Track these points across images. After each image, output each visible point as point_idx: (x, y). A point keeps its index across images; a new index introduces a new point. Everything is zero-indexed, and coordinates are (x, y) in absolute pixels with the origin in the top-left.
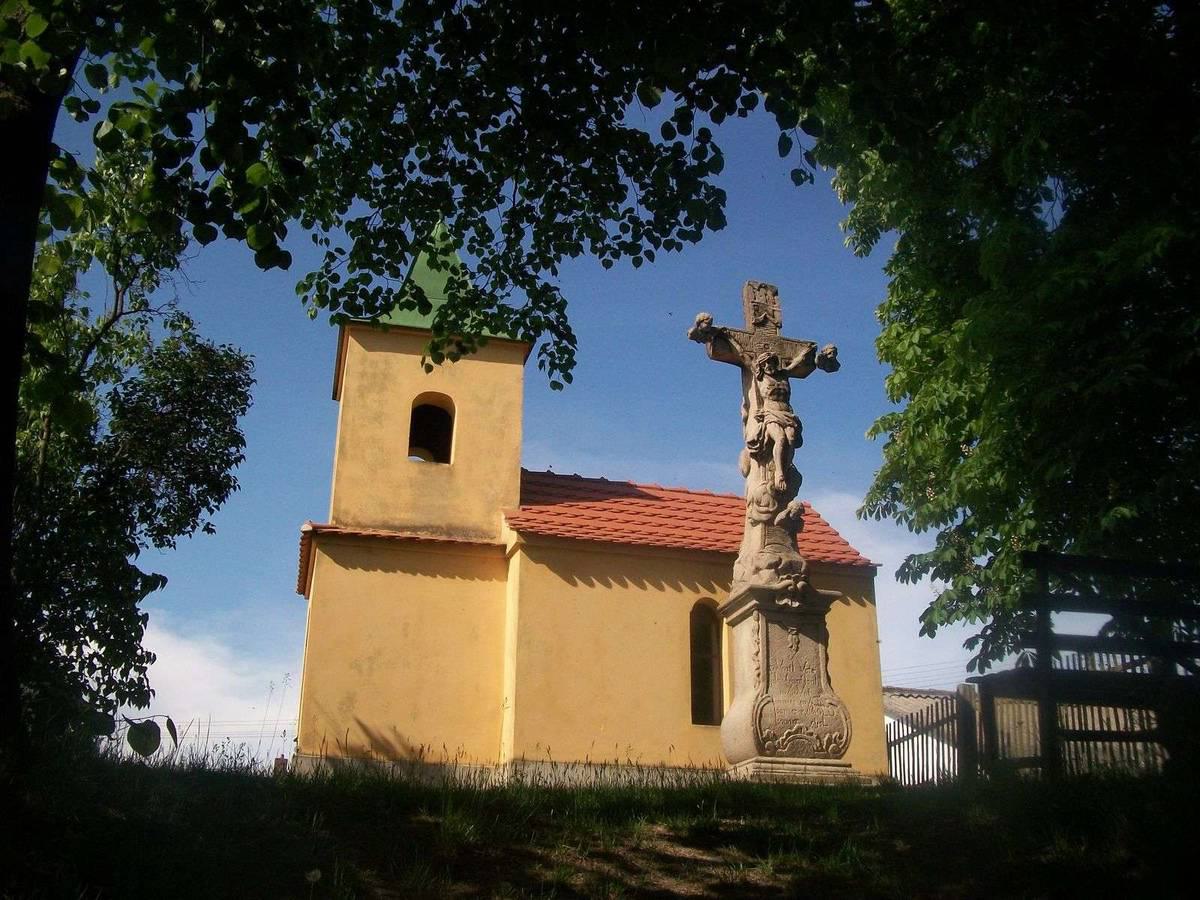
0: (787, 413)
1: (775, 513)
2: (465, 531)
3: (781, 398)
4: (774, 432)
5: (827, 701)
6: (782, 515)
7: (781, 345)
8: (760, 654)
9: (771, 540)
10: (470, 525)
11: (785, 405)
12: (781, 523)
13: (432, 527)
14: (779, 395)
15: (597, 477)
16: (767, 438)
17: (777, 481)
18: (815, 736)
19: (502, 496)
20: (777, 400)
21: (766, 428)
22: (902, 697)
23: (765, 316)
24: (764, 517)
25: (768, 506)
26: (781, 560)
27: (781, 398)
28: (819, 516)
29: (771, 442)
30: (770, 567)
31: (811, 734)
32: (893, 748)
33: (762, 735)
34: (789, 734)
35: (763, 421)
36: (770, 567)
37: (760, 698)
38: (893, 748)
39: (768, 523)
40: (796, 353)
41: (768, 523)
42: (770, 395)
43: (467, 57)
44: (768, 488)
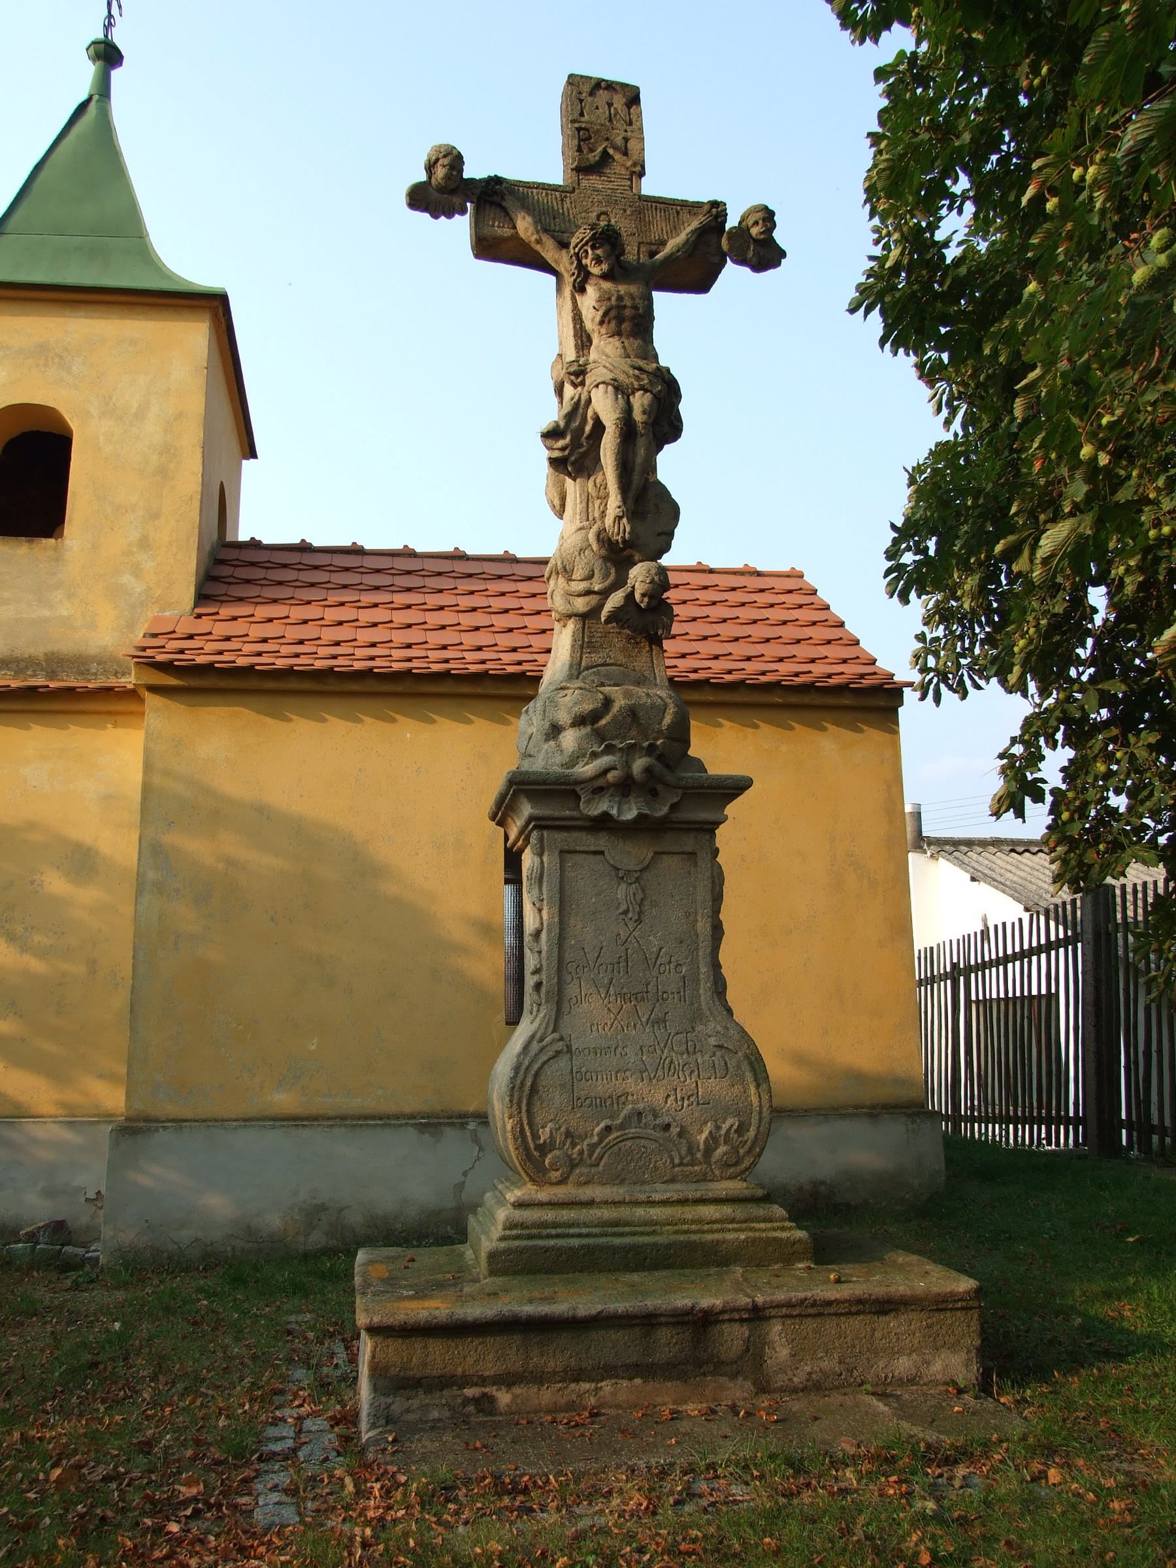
0: (641, 363)
1: (605, 593)
2: (80, 663)
3: (626, 326)
4: (604, 406)
5: (712, 1041)
6: (615, 600)
7: (639, 212)
8: (544, 936)
9: (596, 658)
10: (93, 651)
11: (637, 343)
12: (614, 617)
13: (17, 661)
14: (620, 320)
15: (735, 562)
16: (590, 423)
17: (609, 521)
18: (675, 1130)
19: (159, 592)
20: (618, 333)
21: (589, 401)
22: (1013, 854)
23: (605, 151)
24: (581, 605)
25: (590, 577)
26: (608, 702)
27: (626, 326)
28: (815, 592)
29: (599, 428)
30: (579, 721)
31: (667, 1127)
32: (973, 975)
33: (536, 1136)
34: (608, 1129)
35: (583, 384)
36: (579, 721)
37: (535, 1047)
38: (973, 975)
39: (587, 617)
40: (675, 230)
41: (587, 617)
42: (601, 323)
43: (963, 384)
44: (592, 536)
